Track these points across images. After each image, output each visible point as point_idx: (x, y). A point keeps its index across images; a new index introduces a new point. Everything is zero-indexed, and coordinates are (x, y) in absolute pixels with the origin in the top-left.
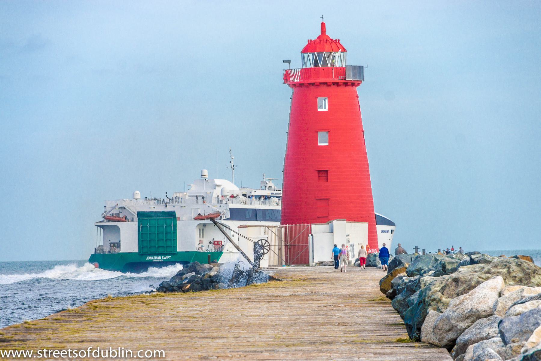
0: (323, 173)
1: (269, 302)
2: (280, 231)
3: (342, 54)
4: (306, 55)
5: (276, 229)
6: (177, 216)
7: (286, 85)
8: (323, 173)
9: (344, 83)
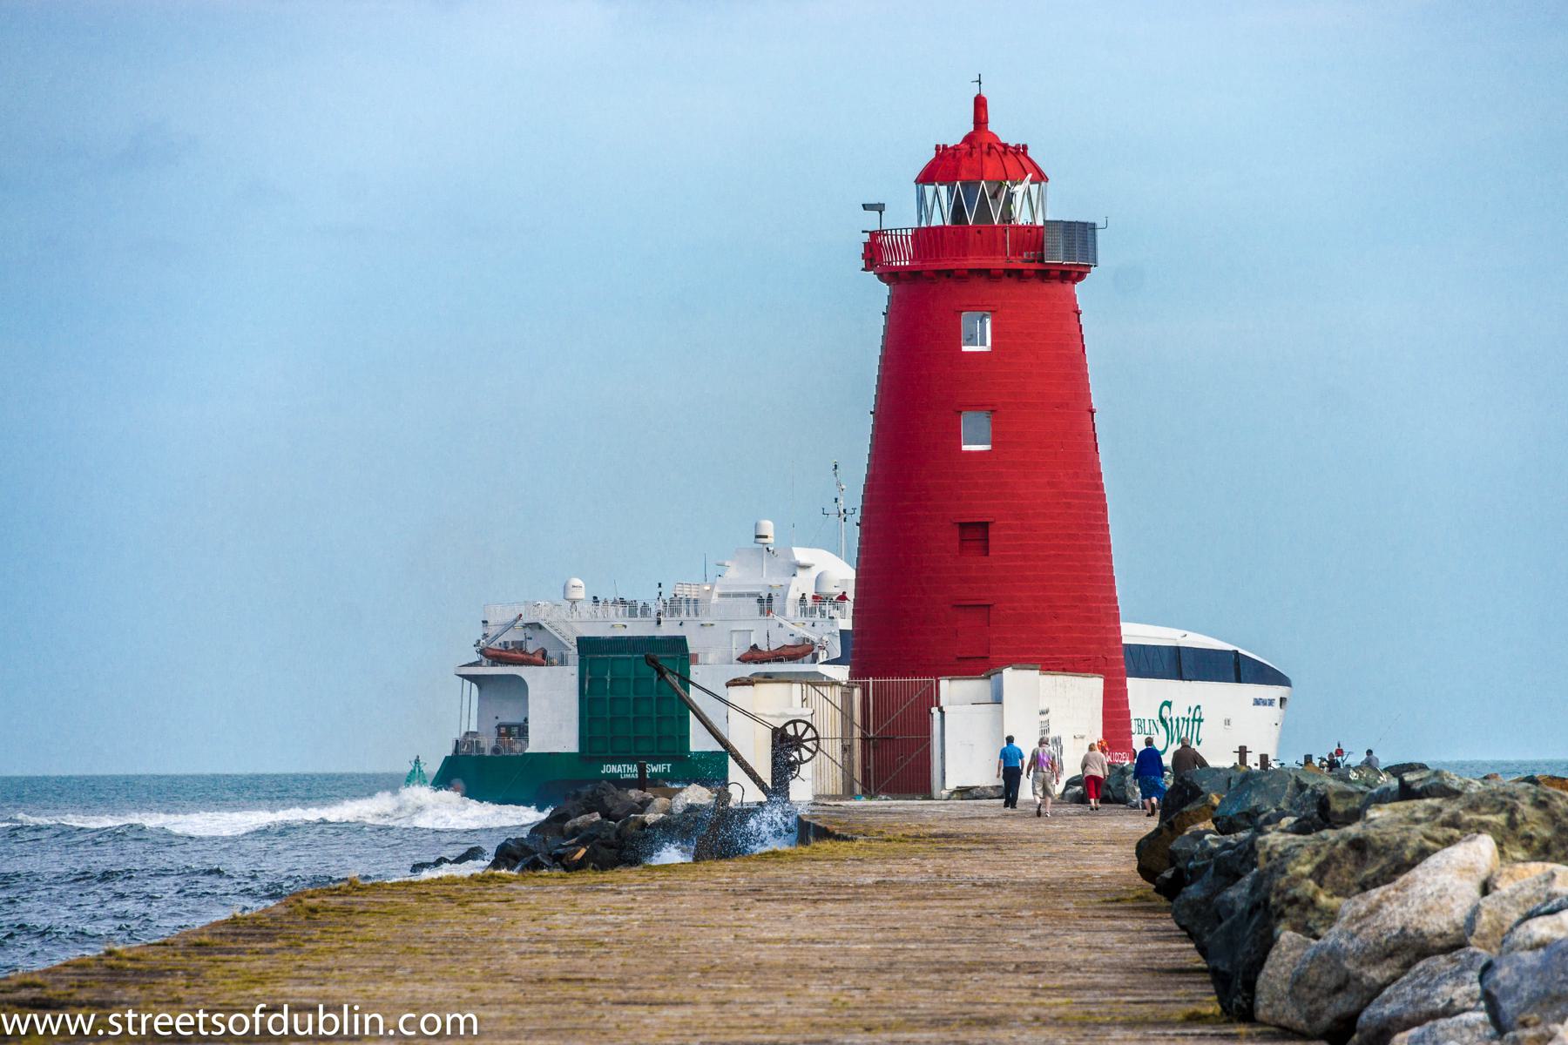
2: (847, 697)
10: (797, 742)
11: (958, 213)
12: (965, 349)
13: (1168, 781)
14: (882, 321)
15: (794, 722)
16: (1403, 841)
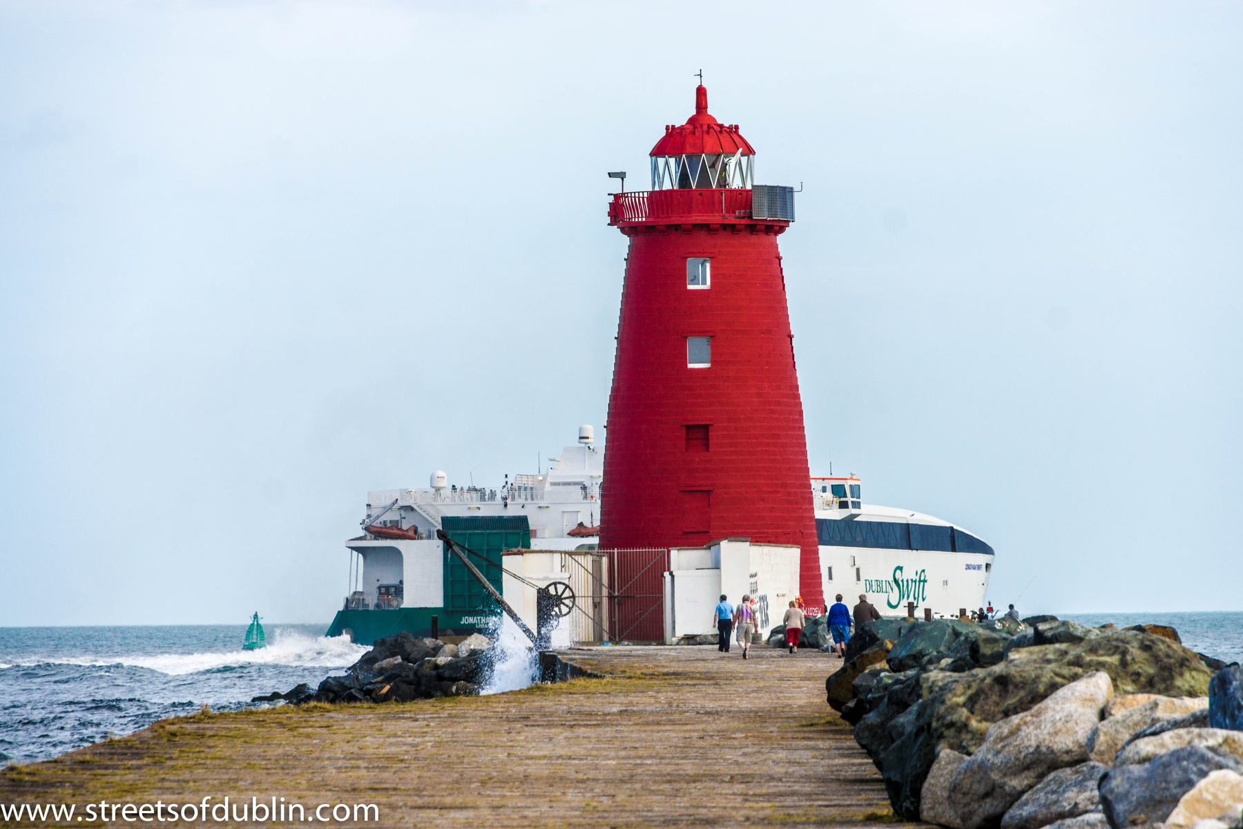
3: (744, 160)
4: (661, 161)
8: (699, 434)
11: (684, 179)
12: (690, 287)
14: (624, 265)
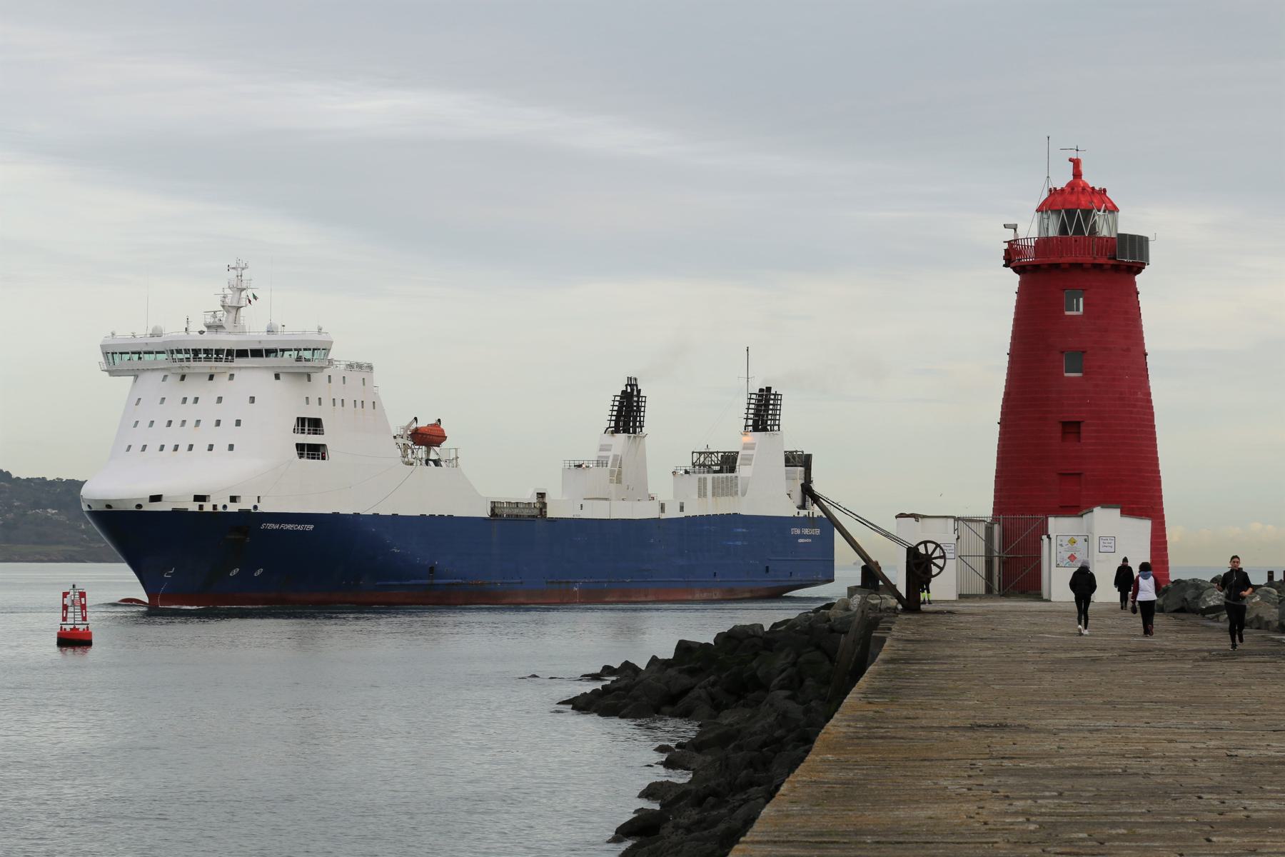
0: (1071, 428)
1: (1021, 662)
2: (989, 530)
5: (983, 525)
6: (485, 513)
7: (1009, 270)
9: (1127, 258)
10: (928, 559)
11: (1063, 230)
12: (1067, 313)
13: (900, 607)
14: (1015, 297)
15: (925, 543)
16: (661, 763)
